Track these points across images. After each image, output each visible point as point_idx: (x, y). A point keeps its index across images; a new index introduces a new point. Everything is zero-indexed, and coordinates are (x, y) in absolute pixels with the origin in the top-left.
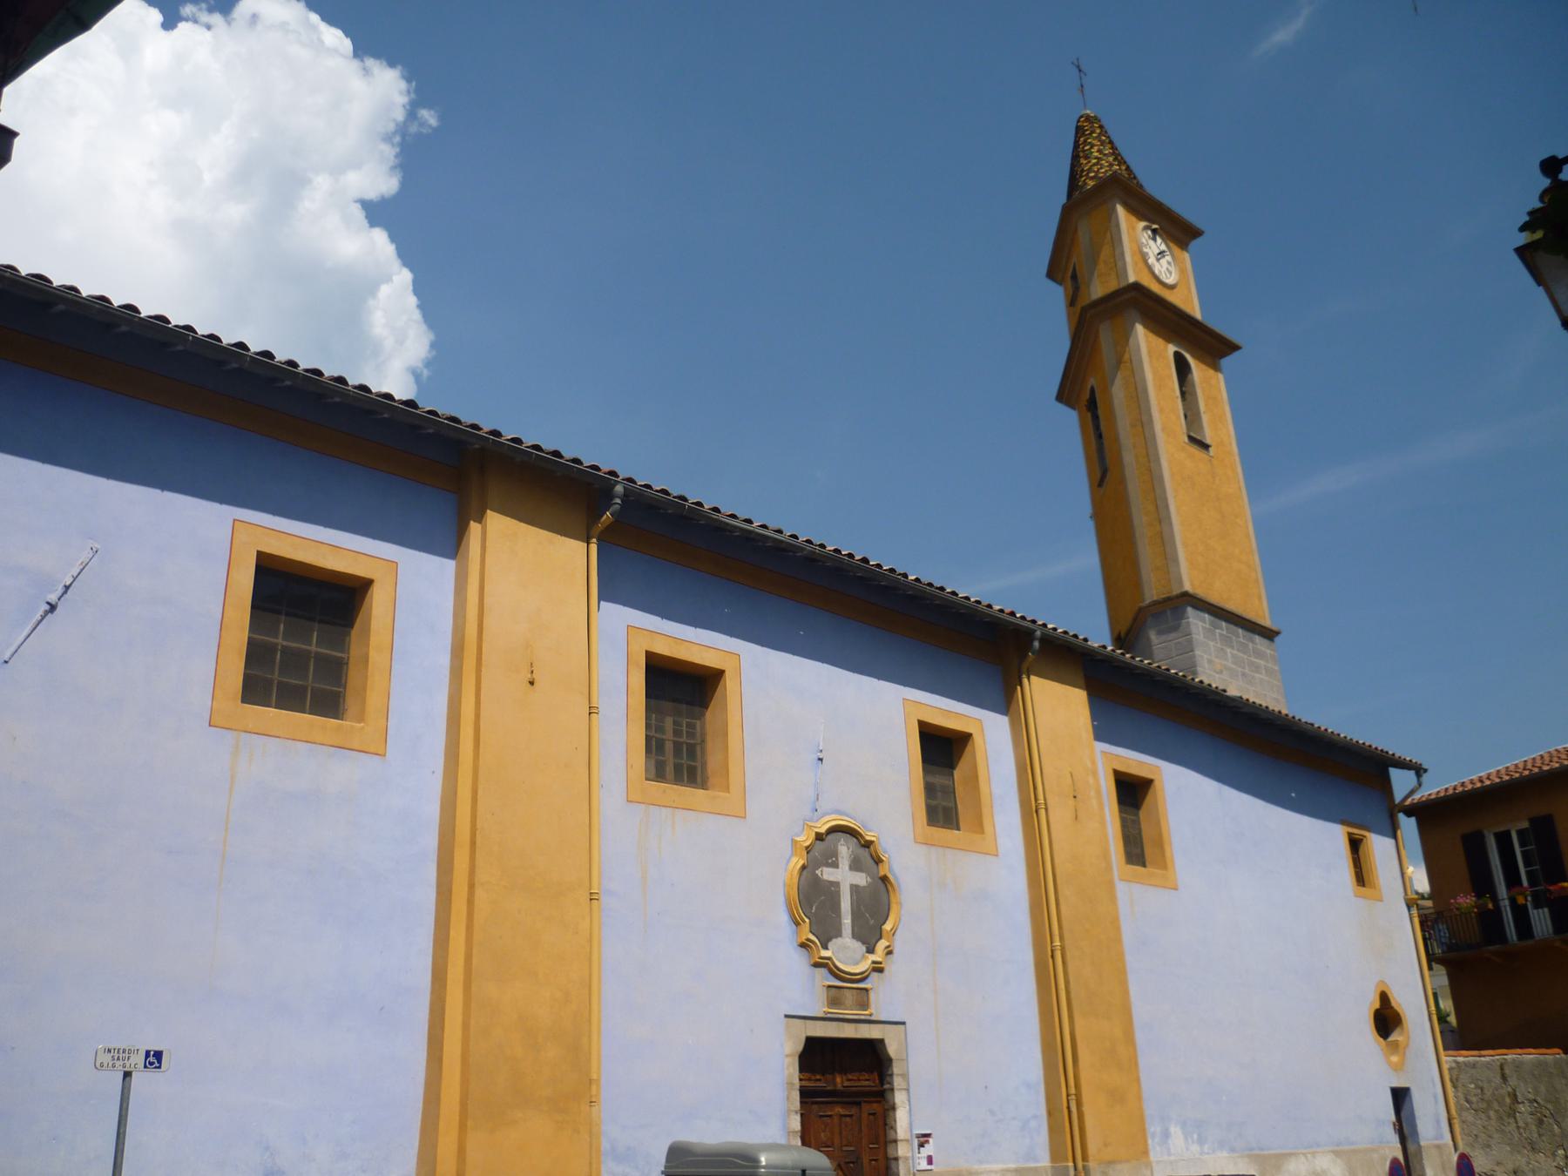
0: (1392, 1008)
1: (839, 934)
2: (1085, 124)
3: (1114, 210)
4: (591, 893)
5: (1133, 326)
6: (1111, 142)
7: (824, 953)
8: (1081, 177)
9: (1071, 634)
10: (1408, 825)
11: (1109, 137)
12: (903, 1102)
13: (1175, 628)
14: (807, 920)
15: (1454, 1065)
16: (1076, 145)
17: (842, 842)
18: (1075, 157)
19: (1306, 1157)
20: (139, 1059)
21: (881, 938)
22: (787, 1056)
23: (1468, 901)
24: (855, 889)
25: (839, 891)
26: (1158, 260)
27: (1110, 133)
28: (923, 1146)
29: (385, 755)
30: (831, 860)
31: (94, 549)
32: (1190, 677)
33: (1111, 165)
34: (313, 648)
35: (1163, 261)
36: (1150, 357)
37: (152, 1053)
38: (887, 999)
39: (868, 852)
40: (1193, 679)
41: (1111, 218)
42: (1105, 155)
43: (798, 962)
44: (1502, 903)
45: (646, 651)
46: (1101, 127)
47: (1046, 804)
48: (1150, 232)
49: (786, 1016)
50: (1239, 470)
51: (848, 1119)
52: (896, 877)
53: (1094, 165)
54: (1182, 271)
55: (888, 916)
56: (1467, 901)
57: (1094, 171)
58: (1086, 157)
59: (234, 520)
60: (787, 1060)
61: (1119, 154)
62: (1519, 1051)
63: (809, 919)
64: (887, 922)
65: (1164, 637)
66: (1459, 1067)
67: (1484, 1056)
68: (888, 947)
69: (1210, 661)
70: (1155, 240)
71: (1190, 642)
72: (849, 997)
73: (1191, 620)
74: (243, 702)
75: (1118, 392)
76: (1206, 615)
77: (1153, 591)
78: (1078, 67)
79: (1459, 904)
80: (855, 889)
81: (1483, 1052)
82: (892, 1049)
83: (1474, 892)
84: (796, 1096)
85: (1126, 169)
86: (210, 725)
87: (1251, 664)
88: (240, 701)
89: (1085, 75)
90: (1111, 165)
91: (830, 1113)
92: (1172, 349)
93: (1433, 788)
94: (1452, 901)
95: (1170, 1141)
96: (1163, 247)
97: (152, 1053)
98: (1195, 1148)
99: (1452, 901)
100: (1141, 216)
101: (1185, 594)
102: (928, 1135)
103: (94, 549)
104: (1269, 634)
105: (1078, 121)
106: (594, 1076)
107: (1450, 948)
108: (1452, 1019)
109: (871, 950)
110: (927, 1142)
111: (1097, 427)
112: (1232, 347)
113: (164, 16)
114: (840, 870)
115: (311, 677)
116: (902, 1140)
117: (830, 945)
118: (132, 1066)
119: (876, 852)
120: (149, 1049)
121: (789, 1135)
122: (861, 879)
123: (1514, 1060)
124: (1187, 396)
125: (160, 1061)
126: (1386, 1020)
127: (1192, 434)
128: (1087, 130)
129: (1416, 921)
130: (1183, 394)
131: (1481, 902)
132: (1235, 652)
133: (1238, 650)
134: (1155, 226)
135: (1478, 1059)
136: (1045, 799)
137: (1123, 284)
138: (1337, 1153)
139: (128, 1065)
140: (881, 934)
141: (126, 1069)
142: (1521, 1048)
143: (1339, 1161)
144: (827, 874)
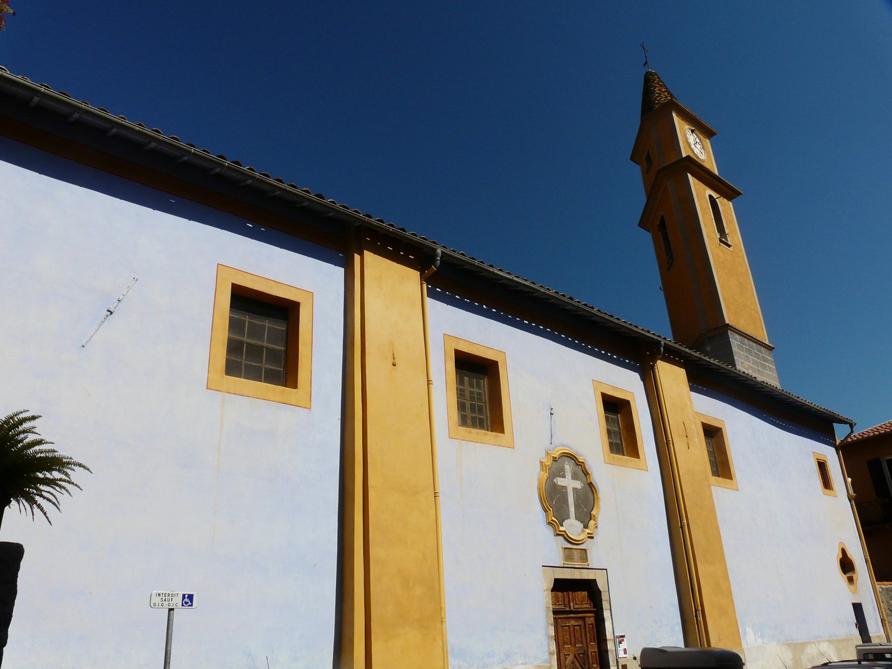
0: (848, 557)
1: (568, 518)
4: (435, 493)
6: (664, 85)
7: (561, 528)
11: (663, 83)
12: (608, 617)
14: (551, 509)
17: (566, 462)
19: (815, 645)
20: (178, 600)
21: (591, 519)
22: (545, 591)
24: (575, 490)
25: (567, 492)
28: (621, 643)
29: (310, 409)
30: (561, 473)
31: (136, 279)
33: (666, 97)
34: (265, 344)
37: (187, 596)
38: (596, 558)
39: (582, 470)
42: (663, 92)
43: (548, 532)
45: (455, 349)
46: (658, 78)
47: (673, 441)
49: (543, 566)
51: (578, 627)
52: (596, 483)
53: (657, 97)
55: (593, 508)
57: (658, 100)
59: (218, 264)
60: (545, 593)
61: (670, 92)
63: (552, 508)
64: (594, 510)
68: (595, 524)
69: (742, 363)
72: (576, 555)
78: (643, 47)
80: (575, 490)
82: (601, 585)
84: (551, 615)
86: (207, 389)
87: (763, 365)
88: (224, 374)
90: (666, 97)
91: (568, 625)
92: (709, 192)
95: (747, 637)
97: (187, 596)
98: (760, 640)
102: (623, 636)
103: (136, 279)
106: (443, 606)
109: (586, 527)
110: (623, 640)
111: (666, 239)
112: (738, 194)
113: (3, 648)
114: (567, 479)
115: (264, 361)
116: (609, 640)
117: (564, 523)
118: (174, 605)
119: (585, 468)
120: (185, 593)
121: (548, 639)
122: (578, 485)
125: (192, 601)
126: (846, 565)
132: (753, 358)
136: (672, 438)
137: (679, 158)
138: (830, 642)
139: (171, 605)
140: (591, 518)
141: (170, 607)
143: (832, 646)
144: (560, 481)
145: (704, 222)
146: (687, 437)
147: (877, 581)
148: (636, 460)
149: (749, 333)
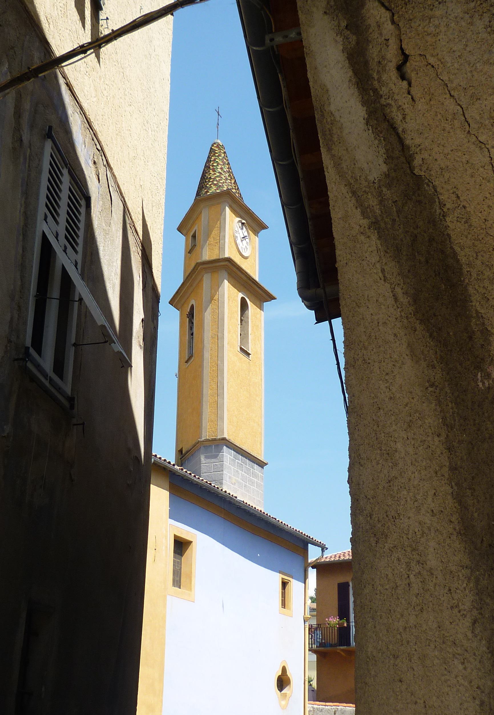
2: (216, 149)
3: (225, 208)
5: (224, 280)
6: (228, 164)
8: (209, 181)
9: (168, 461)
10: (312, 574)
13: (216, 457)
15: (312, 709)
16: (209, 161)
18: (207, 167)
23: (335, 620)
26: (242, 241)
27: (229, 158)
32: (220, 489)
35: (244, 242)
36: (229, 300)
40: (222, 490)
41: (220, 217)
44: (351, 624)
46: (225, 153)
48: (240, 224)
50: (263, 369)
53: (217, 177)
54: (253, 248)
56: (334, 621)
58: (214, 171)
62: (345, 704)
65: (208, 460)
66: (314, 711)
67: (327, 706)
69: (230, 478)
70: (242, 229)
71: (222, 465)
73: (224, 453)
74: (338, 584)
75: (208, 316)
76: (232, 451)
77: (206, 434)
78: (218, 112)
79: (330, 622)
81: (327, 704)
83: (338, 616)
85: (234, 183)
89: (221, 117)
92: (241, 295)
93: (329, 556)
94: (327, 619)
96: (246, 234)
99: (327, 619)
100: (238, 215)
101: (224, 439)
104: (262, 464)
105: (213, 146)
107: (321, 645)
108: (314, 684)
112: (271, 298)
123: (342, 709)
124: (243, 322)
127: (242, 347)
128: (217, 153)
129: (307, 629)
130: (241, 320)
131: (341, 621)
132: (243, 473)
133: (245, 472)
134: (244, 221)
135: (324, 707)
142: (346, 703)
145: (229, 328)
146: (155, 549)
147: (309, 700)
148: (178, 534)
149: (244, 448)
